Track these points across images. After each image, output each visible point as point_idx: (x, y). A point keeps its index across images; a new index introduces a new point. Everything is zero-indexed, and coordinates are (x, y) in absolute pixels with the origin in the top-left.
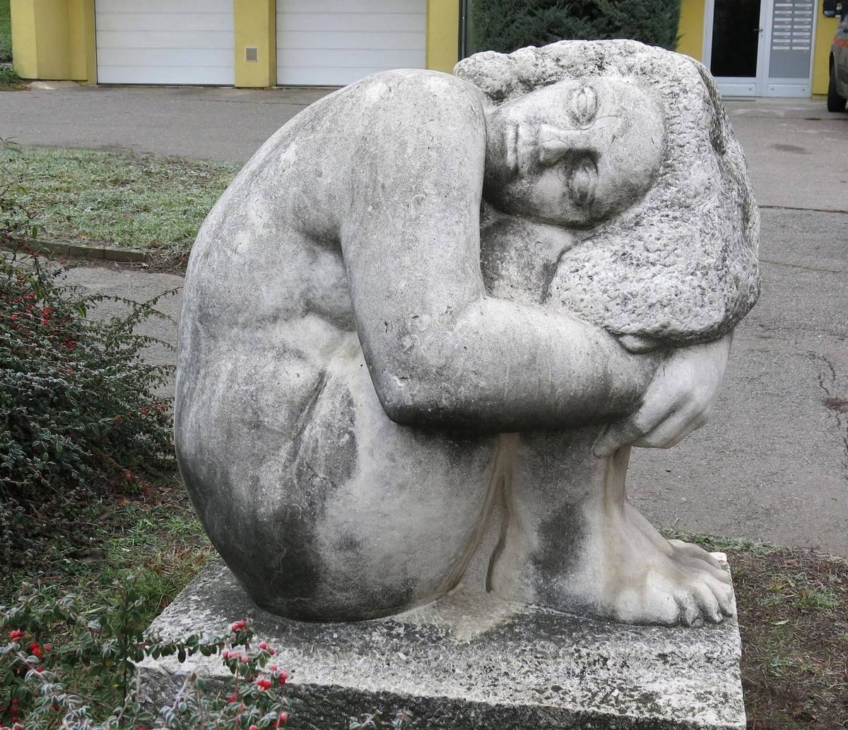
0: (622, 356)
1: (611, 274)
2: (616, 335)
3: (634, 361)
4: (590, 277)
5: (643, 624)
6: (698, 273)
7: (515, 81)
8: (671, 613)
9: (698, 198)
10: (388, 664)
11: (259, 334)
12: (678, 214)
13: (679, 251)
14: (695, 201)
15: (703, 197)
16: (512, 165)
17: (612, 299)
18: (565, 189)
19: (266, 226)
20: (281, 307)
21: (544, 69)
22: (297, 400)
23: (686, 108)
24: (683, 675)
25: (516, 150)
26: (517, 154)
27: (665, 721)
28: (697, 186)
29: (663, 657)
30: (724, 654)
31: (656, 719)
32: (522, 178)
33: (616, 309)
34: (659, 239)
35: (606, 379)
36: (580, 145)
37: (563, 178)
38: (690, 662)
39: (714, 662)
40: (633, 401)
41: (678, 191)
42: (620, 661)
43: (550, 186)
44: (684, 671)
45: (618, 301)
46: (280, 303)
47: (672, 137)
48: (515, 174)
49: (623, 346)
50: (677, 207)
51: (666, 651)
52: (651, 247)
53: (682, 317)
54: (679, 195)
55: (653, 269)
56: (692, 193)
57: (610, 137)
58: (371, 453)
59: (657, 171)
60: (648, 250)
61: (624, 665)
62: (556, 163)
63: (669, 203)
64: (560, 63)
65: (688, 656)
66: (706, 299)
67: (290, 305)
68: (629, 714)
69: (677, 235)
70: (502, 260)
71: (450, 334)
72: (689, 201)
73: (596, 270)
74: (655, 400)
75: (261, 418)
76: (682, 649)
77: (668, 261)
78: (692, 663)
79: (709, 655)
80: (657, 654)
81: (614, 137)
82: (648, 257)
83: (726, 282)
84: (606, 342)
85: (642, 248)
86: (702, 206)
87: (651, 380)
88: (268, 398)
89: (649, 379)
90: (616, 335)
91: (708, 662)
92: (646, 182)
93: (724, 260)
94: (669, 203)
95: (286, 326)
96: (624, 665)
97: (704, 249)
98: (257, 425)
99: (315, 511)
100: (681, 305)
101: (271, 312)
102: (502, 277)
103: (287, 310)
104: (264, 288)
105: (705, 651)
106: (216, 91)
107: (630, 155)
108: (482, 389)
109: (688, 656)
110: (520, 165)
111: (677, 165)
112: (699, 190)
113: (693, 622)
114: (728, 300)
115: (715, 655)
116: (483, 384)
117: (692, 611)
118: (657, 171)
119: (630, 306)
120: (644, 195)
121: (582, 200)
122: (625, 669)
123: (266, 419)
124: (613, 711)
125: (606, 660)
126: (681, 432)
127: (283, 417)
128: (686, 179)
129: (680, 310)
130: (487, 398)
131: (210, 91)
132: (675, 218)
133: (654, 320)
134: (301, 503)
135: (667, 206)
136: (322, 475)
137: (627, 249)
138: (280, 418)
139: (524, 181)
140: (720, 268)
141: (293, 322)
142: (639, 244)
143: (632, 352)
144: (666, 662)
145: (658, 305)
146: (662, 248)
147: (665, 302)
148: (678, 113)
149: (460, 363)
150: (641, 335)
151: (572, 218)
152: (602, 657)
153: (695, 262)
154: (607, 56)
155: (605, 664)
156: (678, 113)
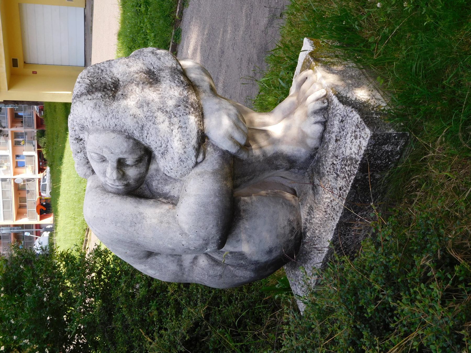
0: (205, 163)
1: (170, 162)
2: (197, 164)
3: (208, 157)
4: (171, 169)
5: (322, 138)
6: (172, 128)
7: (87, 165)
8: (319, 128)
9: (139, 122)
10: (319, 238)
11: (186, 270)
12: (146, 132)
13: (162, 135)
14: (140, 123)
15: (139, 119)
16: (123, 187)
17: (181, 165)
18: (134, 167)
19: (145, 266)
20: (177, 264)
21: (82, 158)
22: (213, 263)
23: (99, 120)
24: (346, 135)
25: (117, 186)
26: (119, 186)
27: (361, 161)
28: (133, 122)
29: (337, 141)
30: (341, 114)
31: (359, 164)
32: (129, 183)
33: (185, 164)
34: (156, 142)
35: (215, 173)
36: (115, 165)
37: (129, 168)
38: (341, 130)
39: (344, 119)
40: (225, 155)
41: (136, 130)
42: (335, 158)
43: (132, 173)
44: (345, 134)
45: (182, 163)
46: (175, 264)
47: (112, 128)
48: (127, 185)
49: (201, 162)
50: (143, 131)
51: (335, 138)
52: (160, 145)
53: (191, 139)
54: (137, 130)
55: (169, 147)
56: (137, 125)
57: (112, 155)
58: (236, 247)
59: (127, 136)
60: (161, 146)
61: (337, 157)
62: (122, 171)
63: (141, 134)
64: (80, 151)
65: (338, 130)
66: (184, 126)
67: (176, 261)
68: (355, 173)
69: (155, 135)
70: (162, 190)
71: (190, 236)
72: (140, 126)
73: (168, 167)
74: (227, 146)
75: (218, 275)
76: (335, 131)
77: (166, 141)
78: (342, 129)
79: (340, 121)
80: (335, 143)
81: (112, 153)
82: (164, 147)
83: (177, 113)
84: (198, 169)
85: (160, 148)
86: (143, 120)
87: (217, 147)
88: (211, 272)
89: (216, 148)
90: (197, 164)
91: (343, 122)
92: (131, 141)
93: (167, 111)
94: (141, 134)
95: (184, 262)
96: (337, 157)
97: (162, 123)
98: (221, 276)
99: (256, 263)
100: (185, 139)
101: (178, 267)
102: (170, 192)
103: (178, 262)
104: (169, 269)
105: (338, 122)
106: (87, 16)
107: (119, 148)
108: (213, 226)
109: (338, 130)
110: (123, 184)
111: (124, 128)
112: (135, 122)
113: (325, 119)
114: (185, 113)
115: (341, 118)
116: (211, 226)
117: (319, 118)
118: (127, 136)
119: (185, 160)
120: (137, 140)
121: (139, 161)
122: (339, 157)
123: (219, 273)
124: (353, 177)
125: (333, 163)
126: (240, 128)
127: (219, 268)
128: (130, 127)
129: (187, 140)
130: (217, 224)
131: (87, 18)
132: (148, 134)
133: (191, 152)
134: (253, 267)
135: (142, 135)
136: (242, 262)
137: (160, 152)
138: (219, 269)
139: (130, 182)
140: (170, 115)
141: (183, 259)
142: (158, 149)
143: (204, 158)
144: (339, 140)
145: (185, 150)
146: (160, 142)
147: (184, 147)
148: (101, 124)
149: (203, 233)
150: (197, 156)
151: (146, 162)
152: (332, 164)
153: (167, 128)
154: (76, 137)
155: (335, 164)
156: (101, 124)
